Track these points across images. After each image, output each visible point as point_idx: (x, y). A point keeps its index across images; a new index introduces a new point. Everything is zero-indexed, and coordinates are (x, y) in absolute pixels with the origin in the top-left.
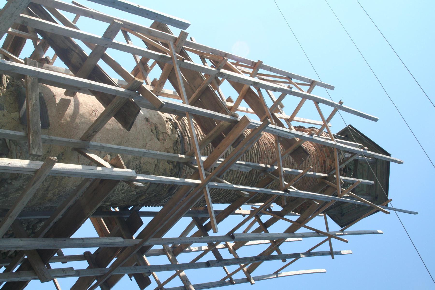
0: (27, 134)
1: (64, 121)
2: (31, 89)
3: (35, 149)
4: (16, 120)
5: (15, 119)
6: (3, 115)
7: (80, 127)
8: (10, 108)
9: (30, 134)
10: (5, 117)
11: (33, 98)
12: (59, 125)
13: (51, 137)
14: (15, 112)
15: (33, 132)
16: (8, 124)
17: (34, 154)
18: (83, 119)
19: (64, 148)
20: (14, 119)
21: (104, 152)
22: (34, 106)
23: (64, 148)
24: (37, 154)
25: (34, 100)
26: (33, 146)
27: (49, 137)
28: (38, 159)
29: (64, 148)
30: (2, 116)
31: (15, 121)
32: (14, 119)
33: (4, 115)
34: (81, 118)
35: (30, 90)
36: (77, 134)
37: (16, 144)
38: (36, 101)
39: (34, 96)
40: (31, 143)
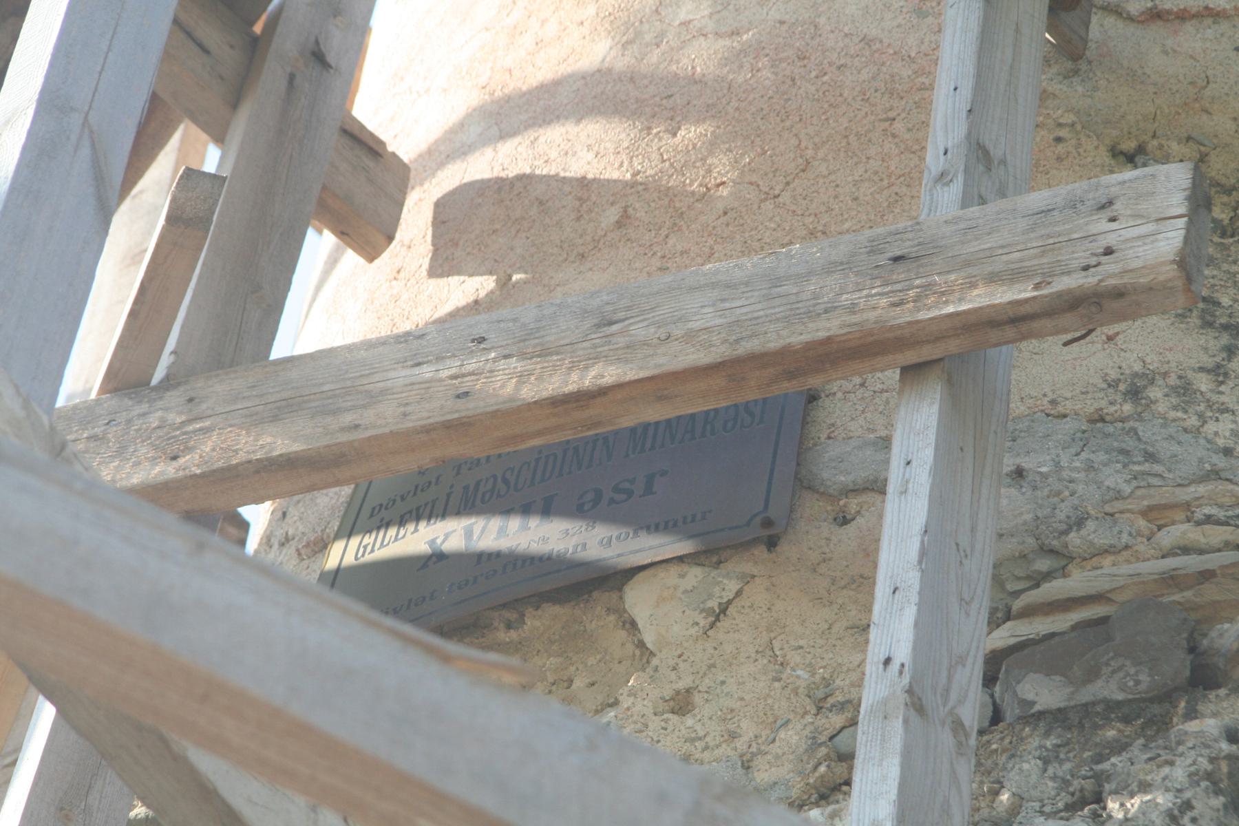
0: (913, 372)
1: (722, 167)
2: (335, 412)
3: (1111, 240)
4: (732, 586)
5: (713, 604)
6: (674, 718)
7: (782, 23)
8: (579, 683)
9: (923, 315)
10: (697, 699)
11: (446, 373)
12: (769, 205)
13: (934, 161)
14: (632, 625)
15: (884, 302)
16: (795, 658)
17: (1186, 239)
18: (683, 15)
19: (1063, 133)
20: (724, 609)
21: (1013, 372)
22: (544, 353)
23: (1059, 140)
24: (1182, 210)
25: (469, 368)
26: (1076, 264)
27: (943, 178)
28: (1219, 366)
29: (1059, 140)
30: (689, 721)
31: (739, 593)
32: (724, 609)
33: (681, 704)
34: (661, 35)
35: (348, 419)
36: (867, 41)
37: (1043, 564)
38: (482, 340)
39: (427, 372)
40: (1037, 287)
